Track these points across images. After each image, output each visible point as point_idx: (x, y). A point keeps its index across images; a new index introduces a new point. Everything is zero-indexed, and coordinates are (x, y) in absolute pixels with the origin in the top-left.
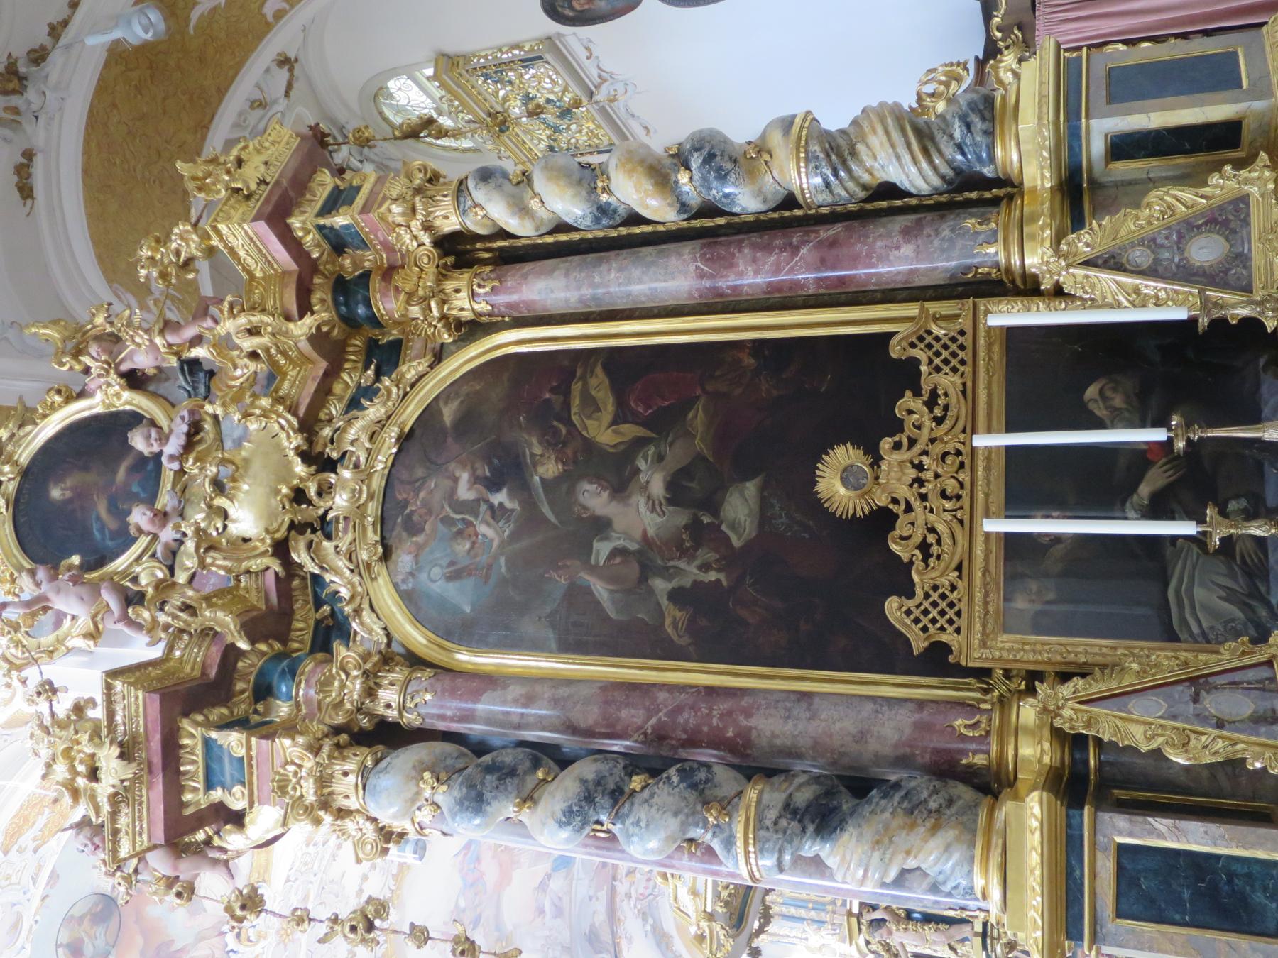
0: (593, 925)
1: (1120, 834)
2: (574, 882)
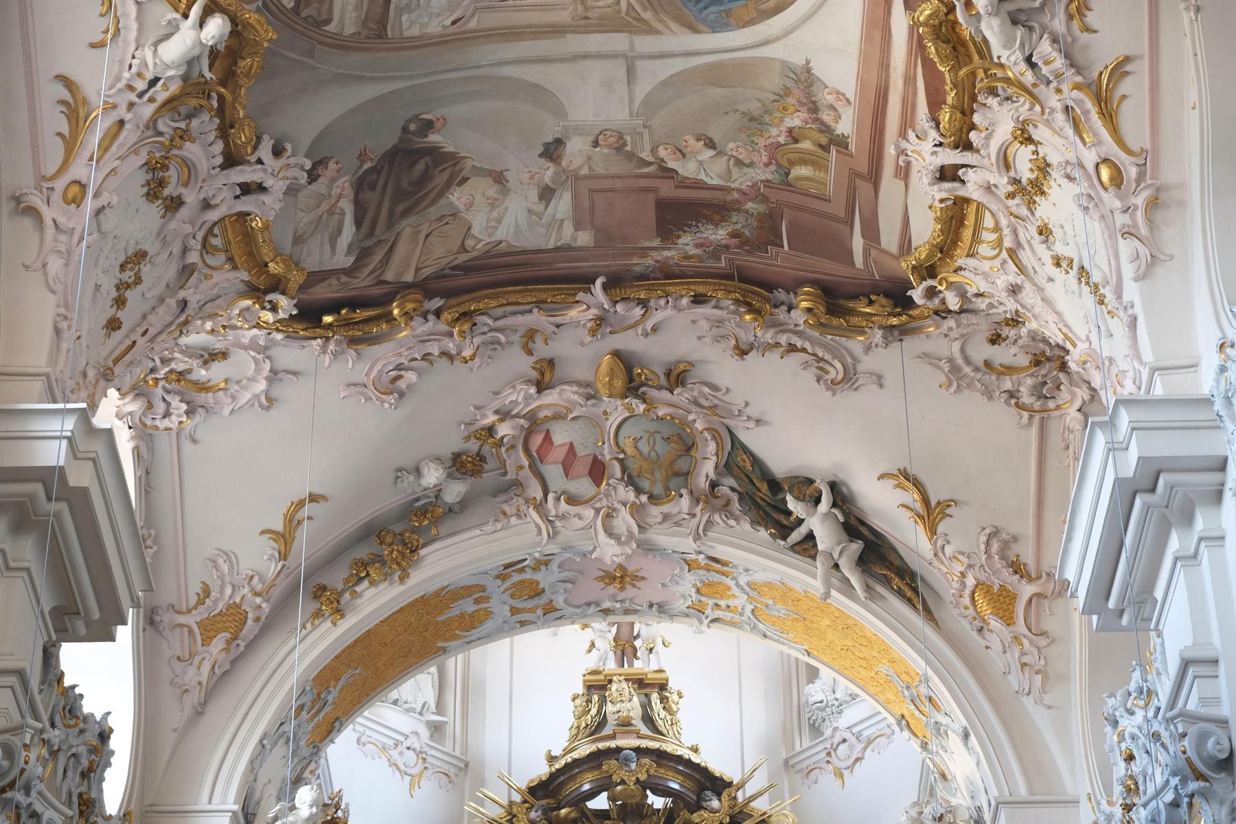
2: (617, 42)
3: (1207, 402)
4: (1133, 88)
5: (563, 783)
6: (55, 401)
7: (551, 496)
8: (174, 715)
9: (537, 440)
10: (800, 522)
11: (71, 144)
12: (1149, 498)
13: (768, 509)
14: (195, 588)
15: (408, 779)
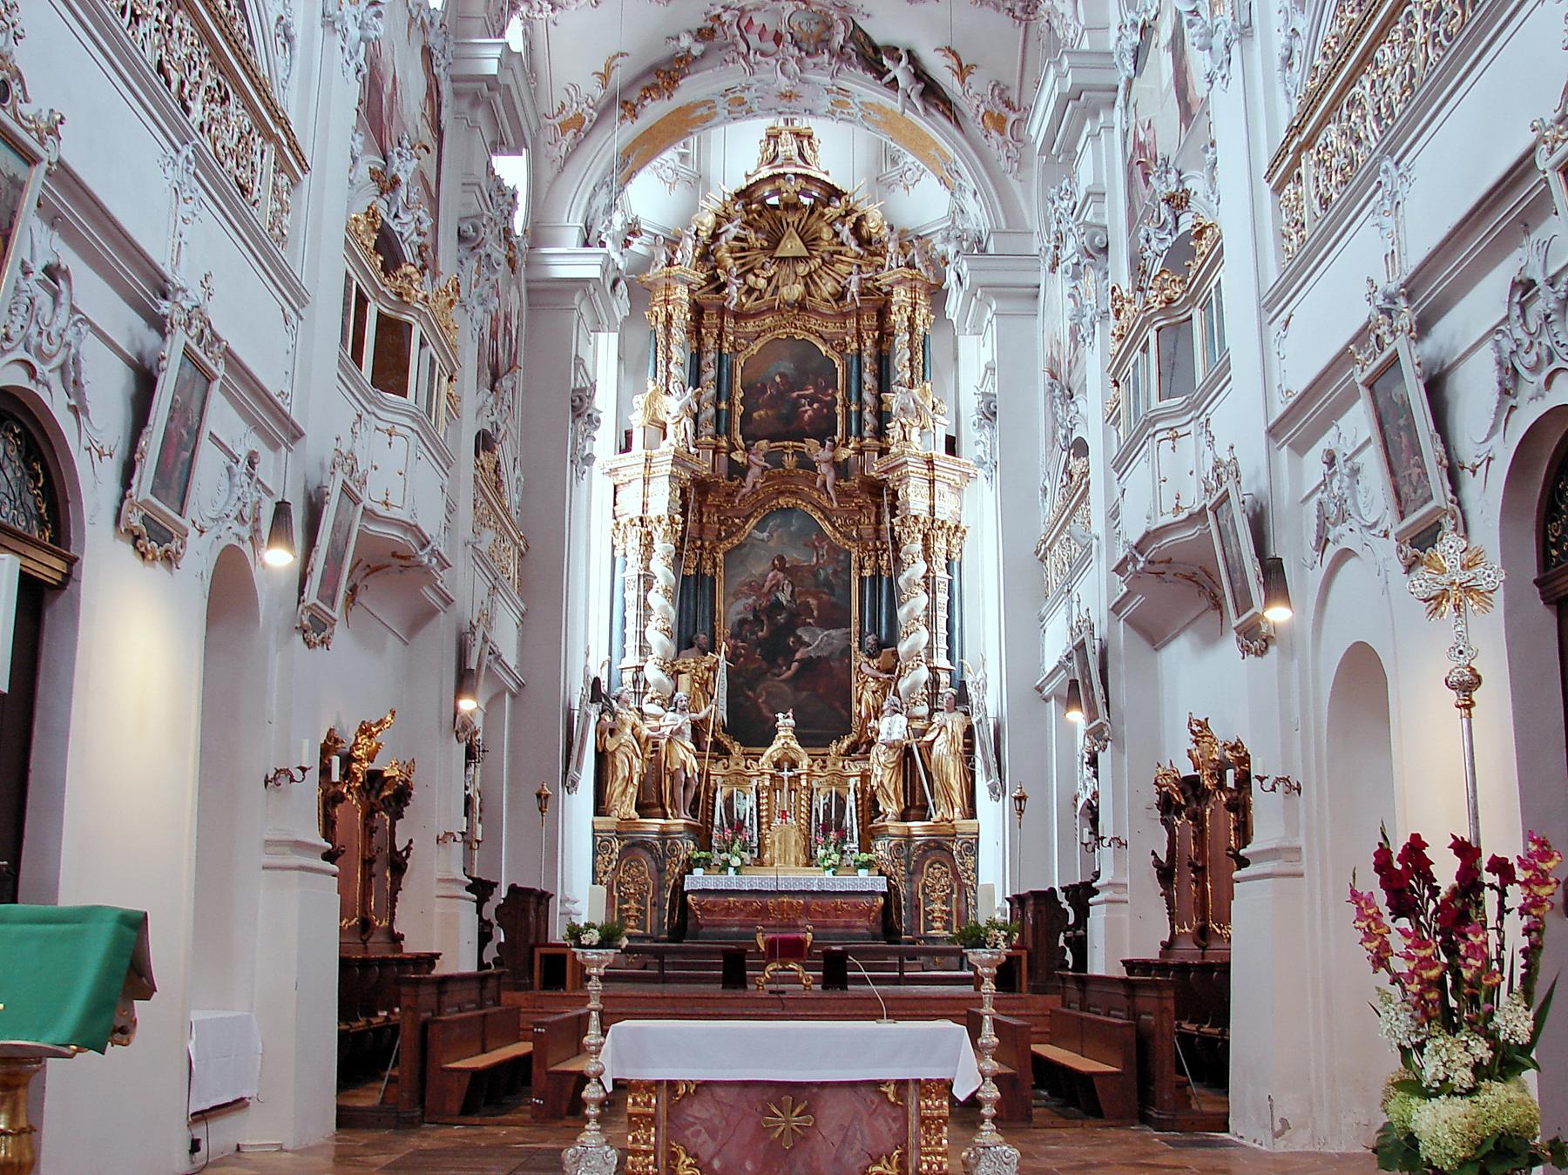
3: (1111, 54)
5: (754, 191)
6: (490, 37)
7: (751, 52)
8: (548, 173)
9: (744, 23)
10: (890, 71)
12: (1076, 103)
13: (872, 62)
14: (557, 105)
15: (668, 185)
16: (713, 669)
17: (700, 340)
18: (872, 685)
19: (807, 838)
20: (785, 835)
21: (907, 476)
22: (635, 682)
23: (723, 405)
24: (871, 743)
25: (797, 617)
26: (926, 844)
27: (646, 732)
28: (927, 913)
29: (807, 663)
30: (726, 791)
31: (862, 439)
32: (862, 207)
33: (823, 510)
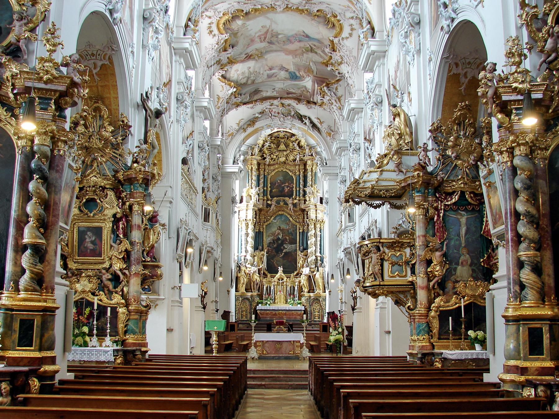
0: (261, 91)
1: (545, 328)
2: (283, 82)
4: (343, 98)
11: (218, 102)
12: (373, 56)
14: (228, 131)
16: (263, 255)
17: (259, 172)
18: (302, 259)
19: (286, 297)
20: (280, 296)
21: (310, 209)
22: (244, 259)
23: (265, 188)
24: (301, 274)
25: (283, 242)
26: (314, 298)
27: (247, 272)
28: (314, 315)
29: (286, 253)
30: (266, 286)
31: (300, 197)
32: (300, 139)
33: (290, 215)
